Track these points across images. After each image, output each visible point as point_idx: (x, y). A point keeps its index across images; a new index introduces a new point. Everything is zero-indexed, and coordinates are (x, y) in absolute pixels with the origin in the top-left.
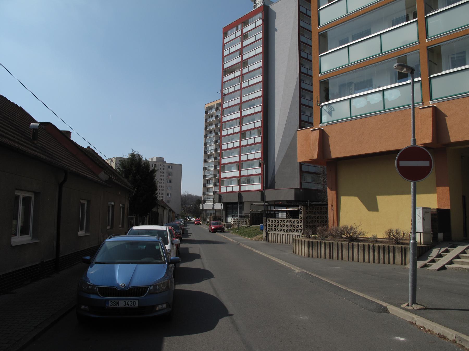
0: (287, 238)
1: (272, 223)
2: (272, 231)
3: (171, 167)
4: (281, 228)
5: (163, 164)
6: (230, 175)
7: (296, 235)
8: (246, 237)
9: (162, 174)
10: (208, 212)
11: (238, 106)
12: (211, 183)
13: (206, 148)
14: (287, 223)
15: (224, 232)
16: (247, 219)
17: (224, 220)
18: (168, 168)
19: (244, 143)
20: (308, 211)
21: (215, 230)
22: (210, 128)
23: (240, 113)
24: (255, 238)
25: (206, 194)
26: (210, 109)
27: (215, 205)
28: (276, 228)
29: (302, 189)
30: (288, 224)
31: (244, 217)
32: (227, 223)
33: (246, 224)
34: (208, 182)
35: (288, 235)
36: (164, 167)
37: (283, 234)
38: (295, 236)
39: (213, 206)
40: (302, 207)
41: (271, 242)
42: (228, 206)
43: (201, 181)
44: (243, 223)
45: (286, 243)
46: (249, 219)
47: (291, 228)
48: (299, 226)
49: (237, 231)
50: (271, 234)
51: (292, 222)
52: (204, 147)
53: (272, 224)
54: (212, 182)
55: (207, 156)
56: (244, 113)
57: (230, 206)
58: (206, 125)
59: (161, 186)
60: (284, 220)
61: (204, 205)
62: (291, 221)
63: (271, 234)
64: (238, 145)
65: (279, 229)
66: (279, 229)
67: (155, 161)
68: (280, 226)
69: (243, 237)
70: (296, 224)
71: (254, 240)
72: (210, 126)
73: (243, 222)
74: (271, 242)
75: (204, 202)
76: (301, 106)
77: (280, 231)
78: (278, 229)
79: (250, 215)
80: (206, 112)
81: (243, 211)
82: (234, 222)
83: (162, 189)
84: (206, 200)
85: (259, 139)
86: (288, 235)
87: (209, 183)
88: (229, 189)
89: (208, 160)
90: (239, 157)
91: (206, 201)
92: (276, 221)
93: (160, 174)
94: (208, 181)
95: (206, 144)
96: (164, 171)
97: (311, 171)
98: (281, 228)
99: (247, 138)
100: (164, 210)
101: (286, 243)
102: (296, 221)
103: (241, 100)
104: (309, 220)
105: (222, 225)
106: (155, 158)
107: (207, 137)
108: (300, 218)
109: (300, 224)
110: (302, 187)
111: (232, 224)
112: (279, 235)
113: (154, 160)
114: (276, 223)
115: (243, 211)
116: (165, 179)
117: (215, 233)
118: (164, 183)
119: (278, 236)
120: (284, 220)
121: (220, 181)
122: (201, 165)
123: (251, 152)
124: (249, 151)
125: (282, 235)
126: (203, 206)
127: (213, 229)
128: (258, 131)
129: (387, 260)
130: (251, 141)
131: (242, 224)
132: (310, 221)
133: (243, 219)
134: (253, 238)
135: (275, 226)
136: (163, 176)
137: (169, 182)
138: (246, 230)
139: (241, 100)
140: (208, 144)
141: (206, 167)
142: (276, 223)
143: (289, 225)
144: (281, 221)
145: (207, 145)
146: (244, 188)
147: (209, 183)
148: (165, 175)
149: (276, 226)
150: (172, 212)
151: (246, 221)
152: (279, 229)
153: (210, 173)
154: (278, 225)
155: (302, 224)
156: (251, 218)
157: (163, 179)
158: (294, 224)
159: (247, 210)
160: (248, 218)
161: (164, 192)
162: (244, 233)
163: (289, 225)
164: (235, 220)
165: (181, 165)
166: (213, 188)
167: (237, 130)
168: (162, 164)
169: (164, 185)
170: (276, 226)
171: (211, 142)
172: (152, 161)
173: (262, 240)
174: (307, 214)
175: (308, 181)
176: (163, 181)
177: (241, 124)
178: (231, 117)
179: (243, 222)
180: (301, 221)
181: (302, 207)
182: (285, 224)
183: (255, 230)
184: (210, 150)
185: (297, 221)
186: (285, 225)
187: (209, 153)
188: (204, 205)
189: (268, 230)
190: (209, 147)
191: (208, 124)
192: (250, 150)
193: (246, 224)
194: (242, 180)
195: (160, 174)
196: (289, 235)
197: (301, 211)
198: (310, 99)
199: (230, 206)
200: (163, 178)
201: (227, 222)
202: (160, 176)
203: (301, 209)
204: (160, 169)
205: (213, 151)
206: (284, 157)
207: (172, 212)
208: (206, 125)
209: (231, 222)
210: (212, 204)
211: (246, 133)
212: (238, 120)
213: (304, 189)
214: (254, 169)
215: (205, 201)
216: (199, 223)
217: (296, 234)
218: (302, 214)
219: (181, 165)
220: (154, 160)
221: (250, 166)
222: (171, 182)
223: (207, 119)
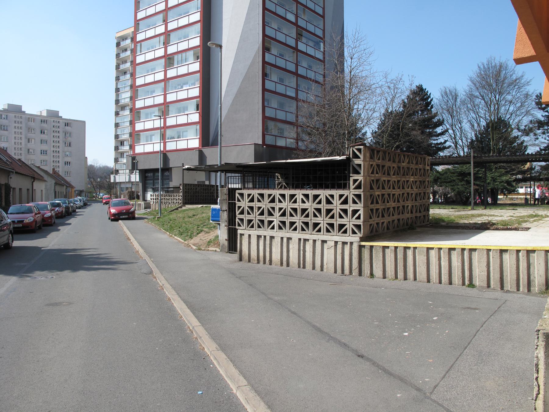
0: (302, 252)
1: (251, 204)
2: (252, 227)
4: (283, 219)
6: (149, 125)
7: (336, 243)
8: (175, 235)
9: (56, 134)
11: (161, 16)
12: (126, 145)
13: (117, 96)
14: (303, 202)
15: (134, 218)
16: (177, 194)
17: (141, 197)
18: (66, 125)
19: (171, 73)
20: (374, 164)
21: (117, 216)
22: (122, 67)
23: (164, 25)
24: (196, 240)
26: (123, 40)
27: (131, 175)
28: (266, 218)
29: (267, 145)
30: (306, 205)
31: (172, 192)
32: (146, 201)
33: (175, 202)
34: (121, 145)
35: (305, 240)
36: (58, 125)
37: (289, 239)
38: (333, 244)
39: (130, 178)
40: (359, 150)
41: (249, 261)
42: (147, 175)
43: (112, 143)
44: (170, 201)
45: (299, 267)
46: (181, 194)
47: (319, 220)
48: (350, 213)
49: (158, 218)
50: (250, 236)
51: (324, 201)
52: (114, 94)
53: (252, 208)
54: (128, 144)
55: (120, 107)
56: (172, 26)
57: (150, 175)
58: (118, 62)
59: (56, 151)
60: (295, 195)
61: (116, 176)
62: (319, 195)
63: (250, 236)
64: (163, 78)
65: (276, 219)
66: (276, 223)
67: (46, 115)
68: (277, 214)
69: (168, 233)
70: (337, 206)
71: (194, 248)
72: (124, 65)
73: (170, 200)
74: (249, 261)
75: (117, 172)
76: (265, 11)
77: (280, 228)
78: (273, 221)
79: (181, 187)
80: (118, 44)
81: (170, 183)
82: (155, 200)
83: (58, 154)
84: (120, 170)
85: (196, 67)
86: (308, 240)
87: (124, 145)
88: (149, 148)
89: (121, 113)
90: (163, 96)
91: (120, 171)
92: (266, 197)
93: (54, 134)
94: (121, 142)
95: (117, 90)
97: (278, 117)
98: (283, 219)
99: (177, 66)
100: (34, 181)
101: (302, 264)
102: (336, 197)
103: (166, 27)
104: (377, 193)
105: (129, 207)
107: (119, 80)
108: (352, 187)
109: (353, 207)
110: (266, 143)
111: (152, 203)
112: (277, 241)
113: (45, 114)
114: (265, 205)
115: (170, 183)
116: (61, 142)
117: (118, 221)
118: (61, 147)
119: (274, 243)
120: (295, 195)
121: (135, 136)
122: (112, 120)
123: (182, 87)
124: (180, 87)
125: (285, 240)
126: (115, 177)
127: (114, 215)
128: (194, 54)
130: (183, 70)
131: (168, 204)
132: (379, 195)
133: (170, 194)
134: (192, 241)
135: (262, 214)
137: (68, 145)
138: (173, 216)
139: (166, 27)
140: (121, 89)
141: (118, 123)
142: (265, 205)
143: (311, 211)
144: (307, 196)
145: (119, 92)
146: (171, 146)
147: (124, 145)
148: (61, 135)
149: (266, 212)
150: (65, 186)
151: (175, 198)
152: (276, 223)
153: (125, 131)
154: (273, 209)
155: (360, 206)
156: (185, 193)
158: (329, 207)
159: (176, 181)
160: (179, 193)
161: (60, 160)
162: (171, 222)
163: (311, 211)
164: (156, 196)
165: (84, 122)
166: (129, 152)
167: (160, 53)
168: (55, 120)
169: (60, 150)
170: (266, 212)
171: (125, 87)
172: (40, 116)
173: (218, 250)
174: (372, 173)
175: (273, 133)
176: (58, 144)
177: (166, 44)
178: (150, 33)
179: (170, 200)
180: (358, 196)
181: (359, 150)
182: (299, 206)
183: (194, 216)
184: (124, 98)
185: (341, 196)
186: (295, 210)
187: (122, 102)
188: (116, 176)
189: (239, 225)
190: (122, 94)
191: (120, 61)
192: (181, 85)
193: (175, 202)
194: (169, 132)
195: (54, 134)
196: (311, 242)
197: (357, 161)
198: (278, 3)
199: (149, 175)
200: (59, 140)
201: (146, 199)
202: (54, 136)
203: (358, 157)
204: (54, 126)
205: (129, 99)
206: (236, 94)
207: (65, 186)
208: (117, 63)
209: (150, 199)
211: (174, 57)
212: (162, 38)
213: (268, 146)
214: (187, 115)
217: (337, 238)
218: (360, 173)
219: (84, 122)
220: (45, 114)
221: (182, 111)
223: (119, 54)
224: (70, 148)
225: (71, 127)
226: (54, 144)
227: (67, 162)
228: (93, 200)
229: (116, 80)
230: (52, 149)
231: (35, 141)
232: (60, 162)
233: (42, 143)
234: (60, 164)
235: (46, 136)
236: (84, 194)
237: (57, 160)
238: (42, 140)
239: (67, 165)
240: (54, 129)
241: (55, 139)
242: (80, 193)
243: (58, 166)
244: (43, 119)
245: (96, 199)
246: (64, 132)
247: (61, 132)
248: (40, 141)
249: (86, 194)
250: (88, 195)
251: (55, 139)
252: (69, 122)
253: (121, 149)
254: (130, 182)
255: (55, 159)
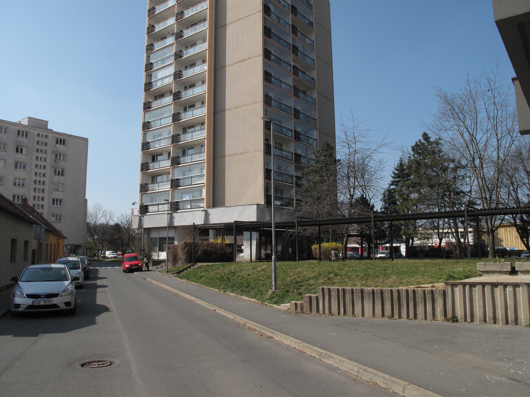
3: (64, 141)
5: (45, 134)
9: (40, 155)
10: (154, 235)
13: (149, 76)
18: (57, 143)
25: (150, 189)
27: (175, 215)
36: (46, 140)
39: (171, 218)
59: (39, 182)
83: (42, 187)
91: (151, 209)
93: (37, 155)
95: (149, 66)
96: (46, 148)
106: (27, 120)
113: (25, 122)
116: (48, 167)
117: (133, 272)
118: (47, 175)
129: (491, 311)
136: (46, 151)
148: (50, 157)
157: (45, 159)
161: (46, 195)
165: (86, 140)
168: (41, 133)
176: (43, 171)
184: (162, 79)
195: (37, 155)
200: (45, 164)
202: (37, 158)
204: (38, 143)
205: (171, 79)
208: (149, 24)
210: (168, 214)
215: (147, 206)
216: (136, 265)
219: (86, 140)
220: (25, 122)
222: (61, 173)
224: (62, 178)
225: (66, 146)
226: (36, 170)
227: (57, 200)
228: (95, 261)
229: (147, 50)
230: (34, 178)
231: (5, 164)
232: (46, 199)
233: (16, 167)
234: (46, 203)
235: (25, 157)
236: (80, 251)
237: (41, 195)
238: (16, 163)
239: (57, 204)
240: (38, 147)
241: (39, 163)
242: (74, 250)
243: (42, 206)
244: (21, 129)
245: (98, 258)
246: (53, 152)
247: (49, 152)
248: (14, 163)
249: (84, 251)
250: (87, 252)
251: (39, 163)
252: (63, 138)
253: (153, 166)
254: (171, 227)
255: (37, 194)
